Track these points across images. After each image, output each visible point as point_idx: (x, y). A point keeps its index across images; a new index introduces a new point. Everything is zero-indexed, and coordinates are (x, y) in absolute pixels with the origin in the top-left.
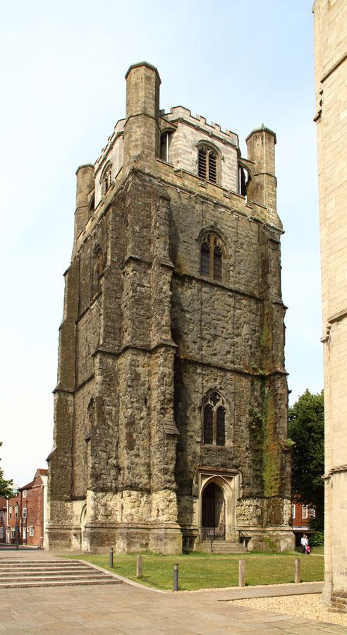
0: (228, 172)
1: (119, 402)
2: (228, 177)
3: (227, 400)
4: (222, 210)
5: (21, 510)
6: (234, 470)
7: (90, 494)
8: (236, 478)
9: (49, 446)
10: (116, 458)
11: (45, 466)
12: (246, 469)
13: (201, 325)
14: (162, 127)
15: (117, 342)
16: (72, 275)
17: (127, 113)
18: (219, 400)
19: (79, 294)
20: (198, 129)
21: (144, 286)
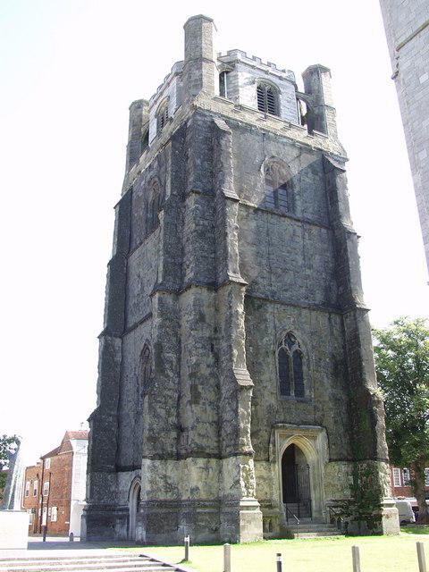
2: (291, 108)
5: (41, 486)
7: (147, 462)
9: (91, 403)
10: (178, 416)
16: (125, 208)
17: (186, 57)
18: (294, 343)
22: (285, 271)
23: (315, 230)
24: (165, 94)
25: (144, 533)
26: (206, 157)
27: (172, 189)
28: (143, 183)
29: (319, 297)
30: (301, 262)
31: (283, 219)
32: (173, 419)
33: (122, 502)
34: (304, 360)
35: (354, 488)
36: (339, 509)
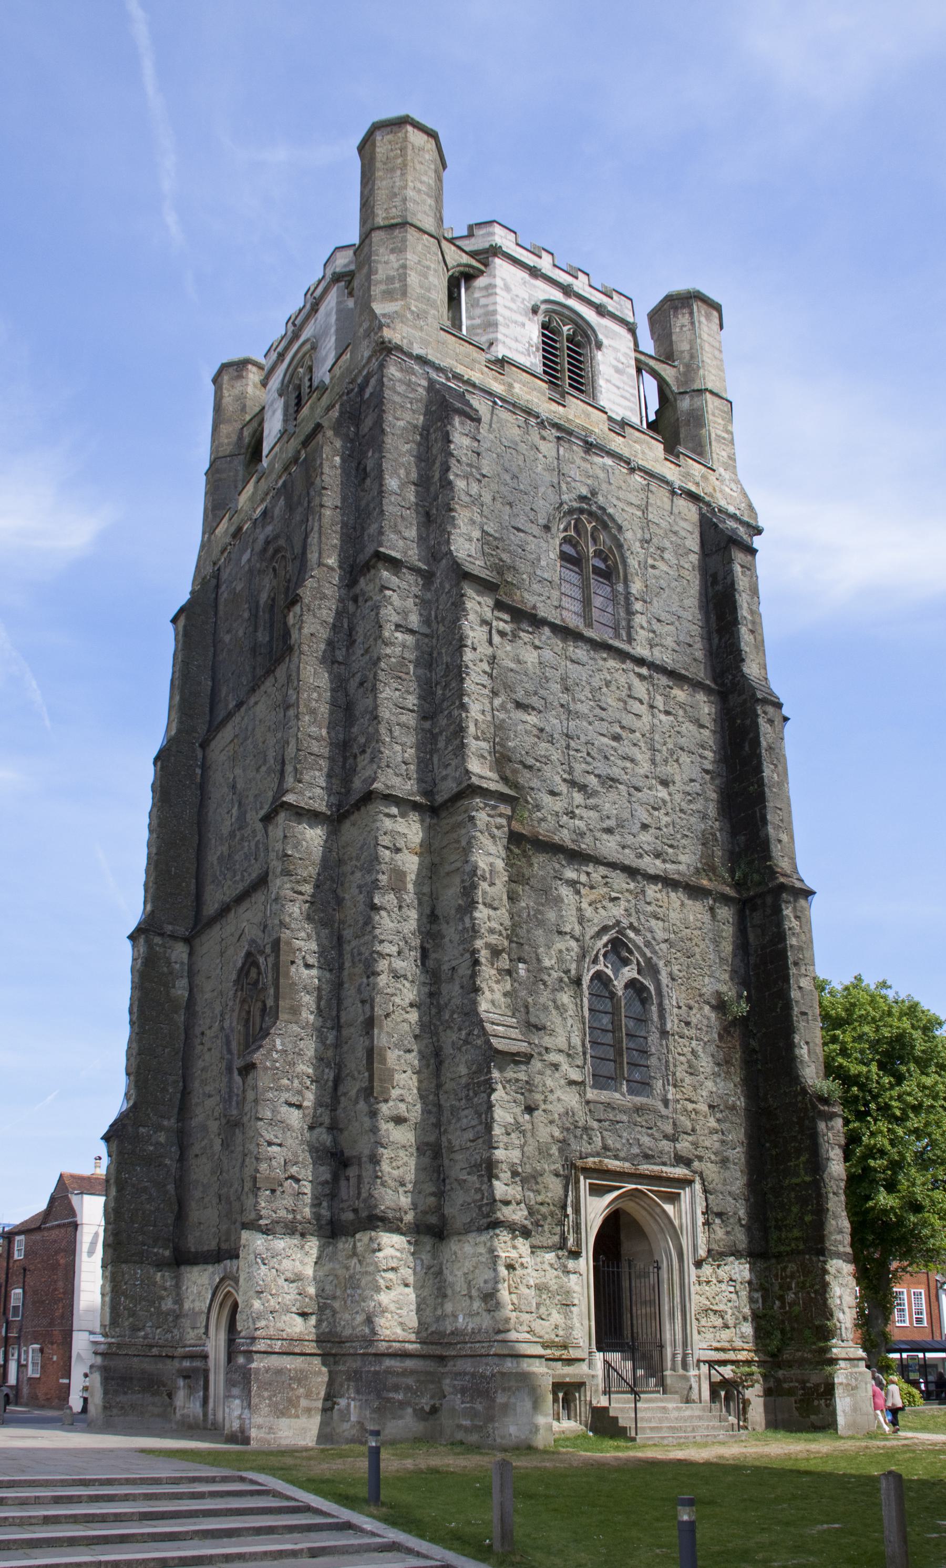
0: (615, 378)
1: (341, 955)
2: (620, 388)
4: (608, 461)
6: (679, 1172)
9: (110, 1098)
12: (710, 1169)
13: (568, 747)
14: (451, 263)
19: (214, 669)
20: (534, 272)
24: (306, 334)
28: (245, 557)
29: (686, 861)
30: (645, 767)
33: (191, 1336)
36: (729, 1367)
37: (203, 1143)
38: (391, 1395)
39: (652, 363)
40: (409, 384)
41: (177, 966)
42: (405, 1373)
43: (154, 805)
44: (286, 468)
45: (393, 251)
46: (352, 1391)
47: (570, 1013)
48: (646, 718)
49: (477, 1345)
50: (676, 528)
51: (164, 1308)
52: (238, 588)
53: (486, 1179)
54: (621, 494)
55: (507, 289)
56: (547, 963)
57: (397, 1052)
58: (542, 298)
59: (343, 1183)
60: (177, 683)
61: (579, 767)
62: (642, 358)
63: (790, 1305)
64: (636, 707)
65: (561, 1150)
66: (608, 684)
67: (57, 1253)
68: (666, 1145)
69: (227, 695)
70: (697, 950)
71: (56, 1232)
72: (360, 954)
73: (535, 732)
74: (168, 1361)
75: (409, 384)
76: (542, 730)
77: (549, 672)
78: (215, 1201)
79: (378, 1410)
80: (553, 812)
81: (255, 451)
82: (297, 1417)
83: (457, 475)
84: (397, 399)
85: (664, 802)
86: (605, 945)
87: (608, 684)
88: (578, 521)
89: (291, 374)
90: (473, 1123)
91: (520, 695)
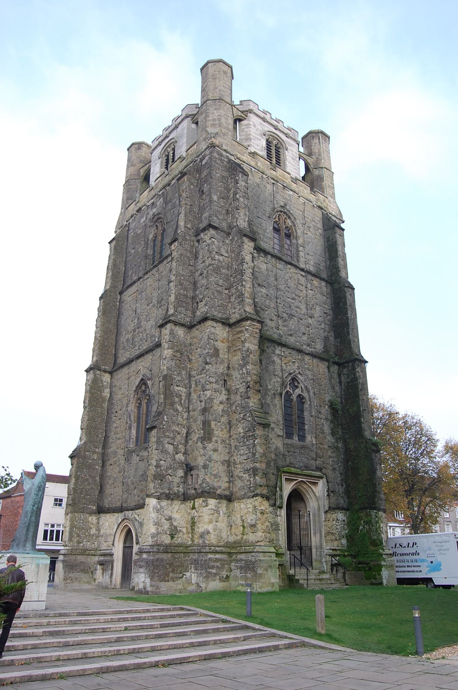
0: (292, 161)
3: (306, 387)
4: (291, 193)
6: (318, 474)
7: (152, 502)
8: (321, 484)
9: (73, 438)
11: (64, 468)
13: (277, 302)
15: (189, 313)
16: (120, 244)
17: (202, 97)
18: (297, 387)
20: (264, 120)
21: (222, 255)
22: (291, 316)
23: (316, 282)
25: (148, 581)
26: (222, 195)
27: (185, 222)
28: (142, 220)
29: (319, 347)
30: (304, 311)
31: (289, 266)
32: (180, 457)
34: (306, 406)
35: (350, 538)
37: (115, 459)
38: (211, 570)
39: (304, 156)
40: (221, 160)
41: (105, 383)
42: (217, 560)
43: (99, 316)
44: (164, 187)
45: (215, 109)
46: (193, 569)
47: (278, 407)
48: (305, 292)
49: (247, 548)
50: (314, 219)
51: (92, 533)
52: (139, 232)
53: (252, 476)
54: (295, 206)
55: (255, 126)
56: (269, 387)
57: (215, 423)
58: (267, 130)
59: (189, 477)
60: (110, 267)
61: (281, 310)
62: (301, 154)
63: (361, 531)
64: (301, 288)
65: (274, 464)
66: (291, 278)
67: (18, 507)
68: (312, 462)
69: (132, 274)
70: (323, 383)
71: (19, 498)
72: (200, 382)
73: (265, 296)
74: (93, 557)
75: (221, 160)
76: (267, 295)
77: (270, 273)
78: (121, 484)
79: (207, 577)
80: (273, 328)
81: (147, 178)
82: (168, 581)
83: (240, 196)
84: (216, 165)
85: (311, 325)
86: (290, 381)
87: (291, 278)
88: (279, 215)
89: (165, 149)
90: (246, 452)
91: (260, 281)
